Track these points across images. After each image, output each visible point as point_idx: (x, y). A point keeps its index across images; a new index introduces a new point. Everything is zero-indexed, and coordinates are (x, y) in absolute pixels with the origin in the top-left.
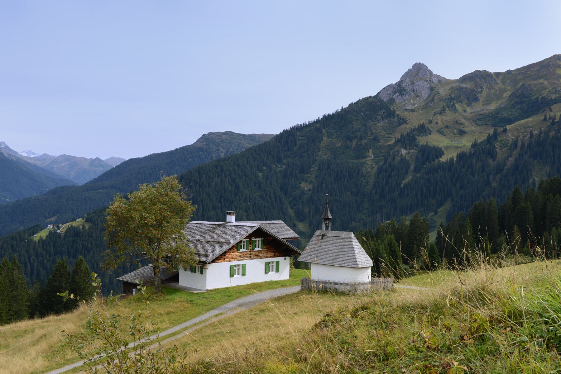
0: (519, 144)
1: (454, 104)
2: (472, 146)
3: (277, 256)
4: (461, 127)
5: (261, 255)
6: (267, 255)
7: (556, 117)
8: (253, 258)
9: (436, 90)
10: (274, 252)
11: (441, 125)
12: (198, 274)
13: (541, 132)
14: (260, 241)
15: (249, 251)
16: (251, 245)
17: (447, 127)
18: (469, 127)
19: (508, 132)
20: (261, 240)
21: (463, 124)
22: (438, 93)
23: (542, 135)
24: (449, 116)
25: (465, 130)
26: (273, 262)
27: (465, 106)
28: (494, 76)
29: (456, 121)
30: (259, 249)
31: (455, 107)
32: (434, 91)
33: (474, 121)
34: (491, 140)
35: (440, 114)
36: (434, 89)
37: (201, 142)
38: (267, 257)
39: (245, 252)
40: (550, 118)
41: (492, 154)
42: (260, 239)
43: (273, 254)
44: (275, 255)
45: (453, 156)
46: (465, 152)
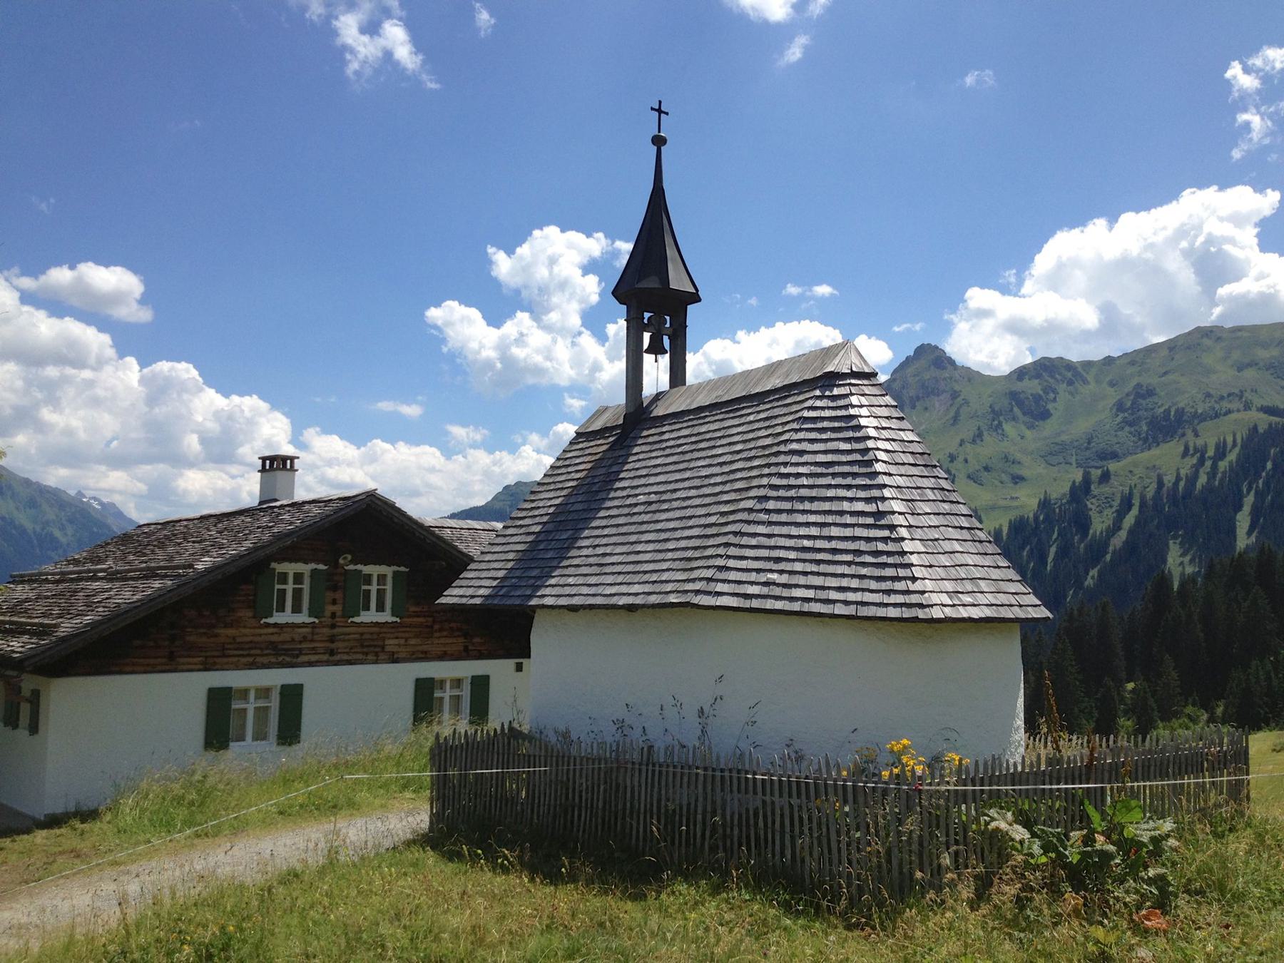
0: (1136, 502)
1: (1000, 424)
2: (1039, 506)
3: (480, 656)
4: (1017, 470)
5: (391, 644)
6: (425, 648)
7: (1209, 449)
8: (345, 657)
9: (963, 397)
10: (465, 636)
11: (974, 465)
12: (22, 733)
13: (1178, 478)
14: (389, 580)
15: (328, 621)
16: (339, 595)
17: (987, 469)
18: (1033, 468)
19: (1112, 477)
20: (395, 573)
21: (1019, 463)
22: (966, 402)
23: (1182, 484)
24: (990, 448)
25: (1024, 475)
26: (458, 683)
27: (1023, 427)
28: (1080, 369)
29: (1006, 457)
30: (386, 617)
31: (1003, 430)
32: (958, 399)
33: (1043, 457)
34: (1080, 492)
35: (974, 442)
36: (959, 395)
37: (501, 500)
38: (425, 657)
39: (304, 625)
40: (1196, 450)
41: (1082, 523)
42: (388, 570)
43: (457, 644)
44: (466, 649)
45: (1001, 525)
46: (1026, 516)
